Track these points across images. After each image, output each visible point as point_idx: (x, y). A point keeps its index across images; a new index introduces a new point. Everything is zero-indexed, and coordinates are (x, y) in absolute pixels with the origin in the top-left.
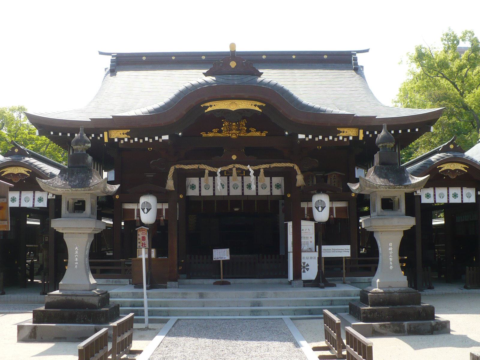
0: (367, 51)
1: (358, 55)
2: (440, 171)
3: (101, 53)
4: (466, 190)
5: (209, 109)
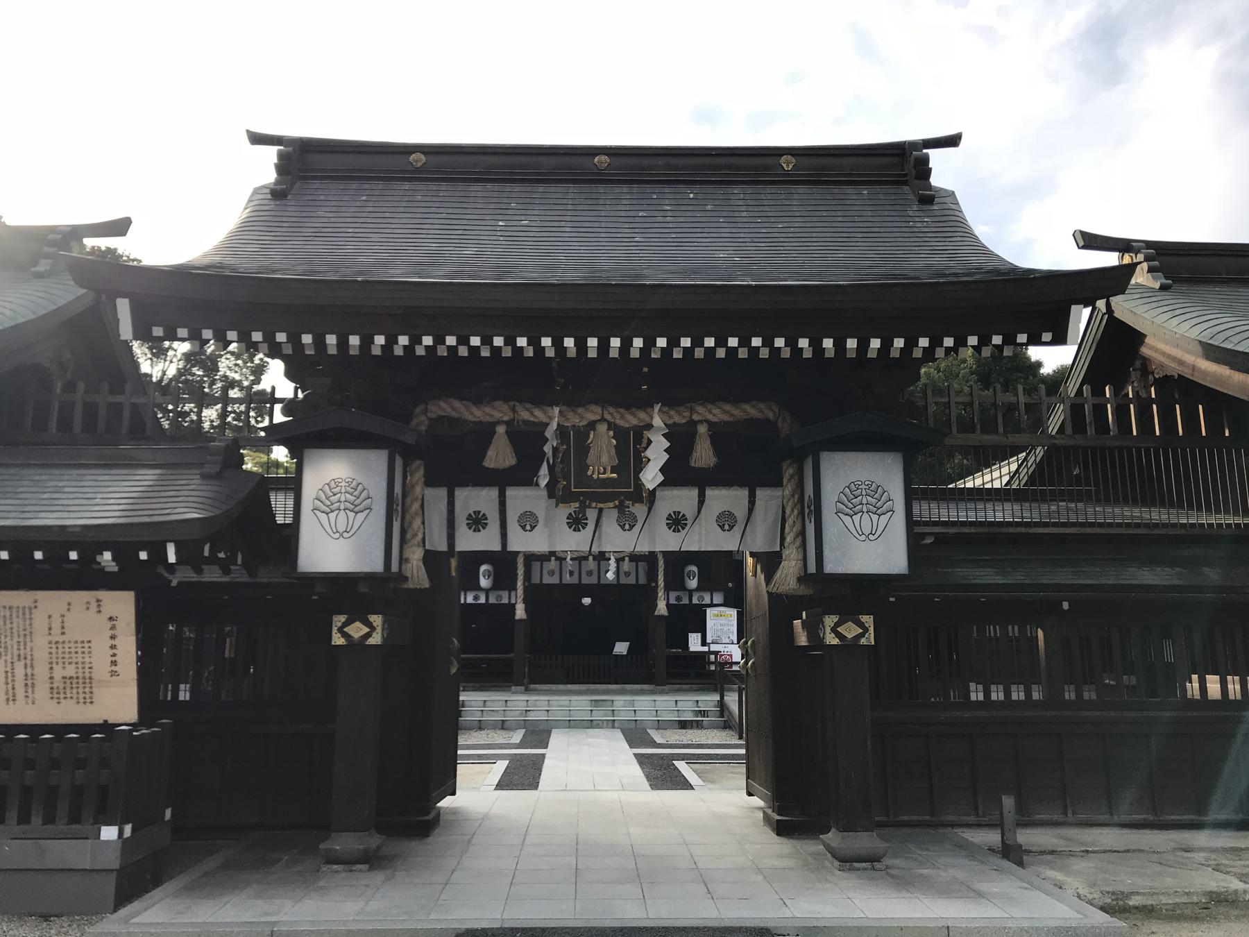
0: (952, 141)
1: (935, 155)
3: (258, 139)
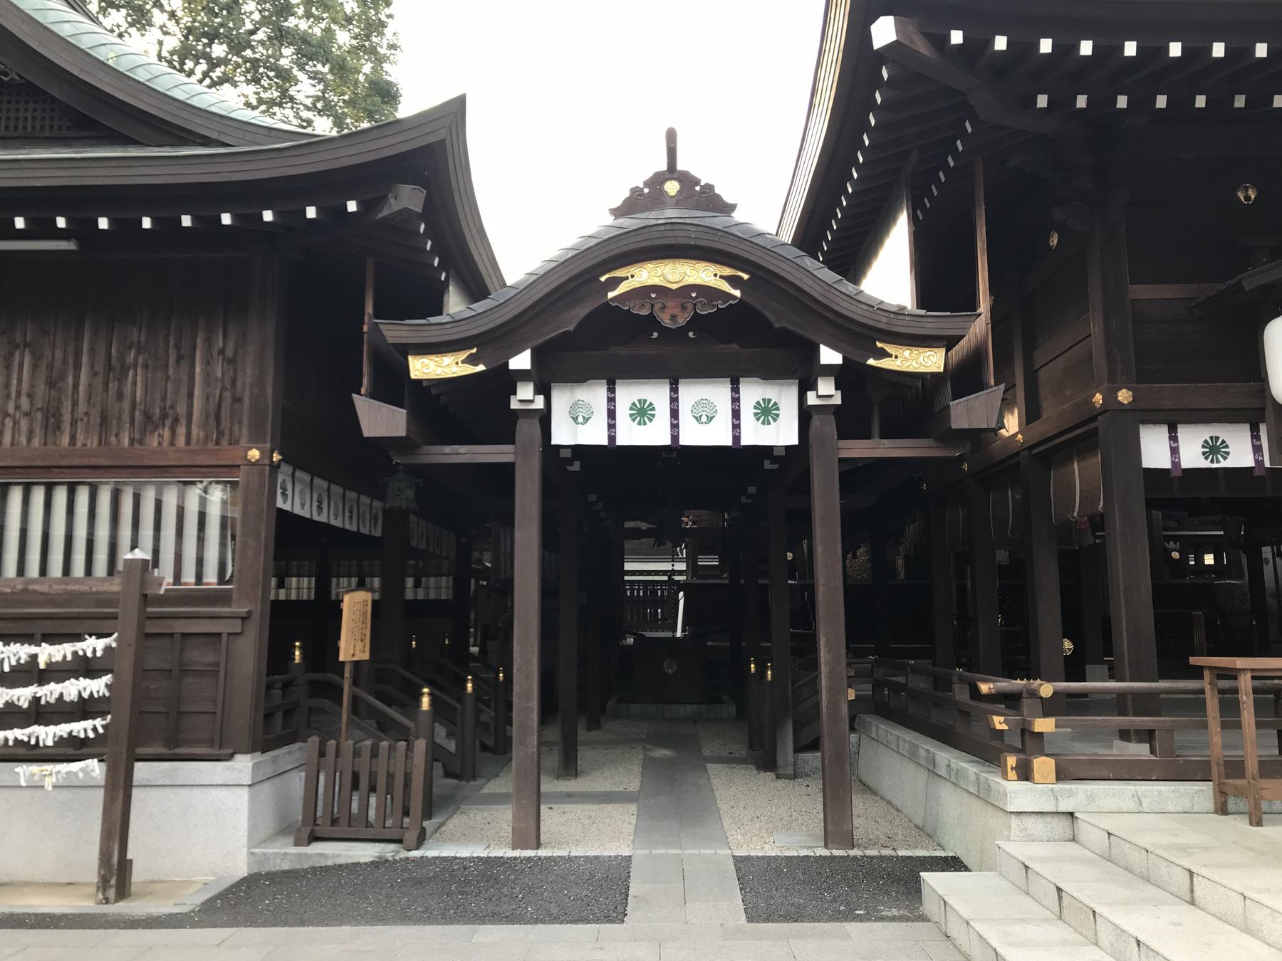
2: (611, 295)
4: (752, 392)
5: (623, 288)
